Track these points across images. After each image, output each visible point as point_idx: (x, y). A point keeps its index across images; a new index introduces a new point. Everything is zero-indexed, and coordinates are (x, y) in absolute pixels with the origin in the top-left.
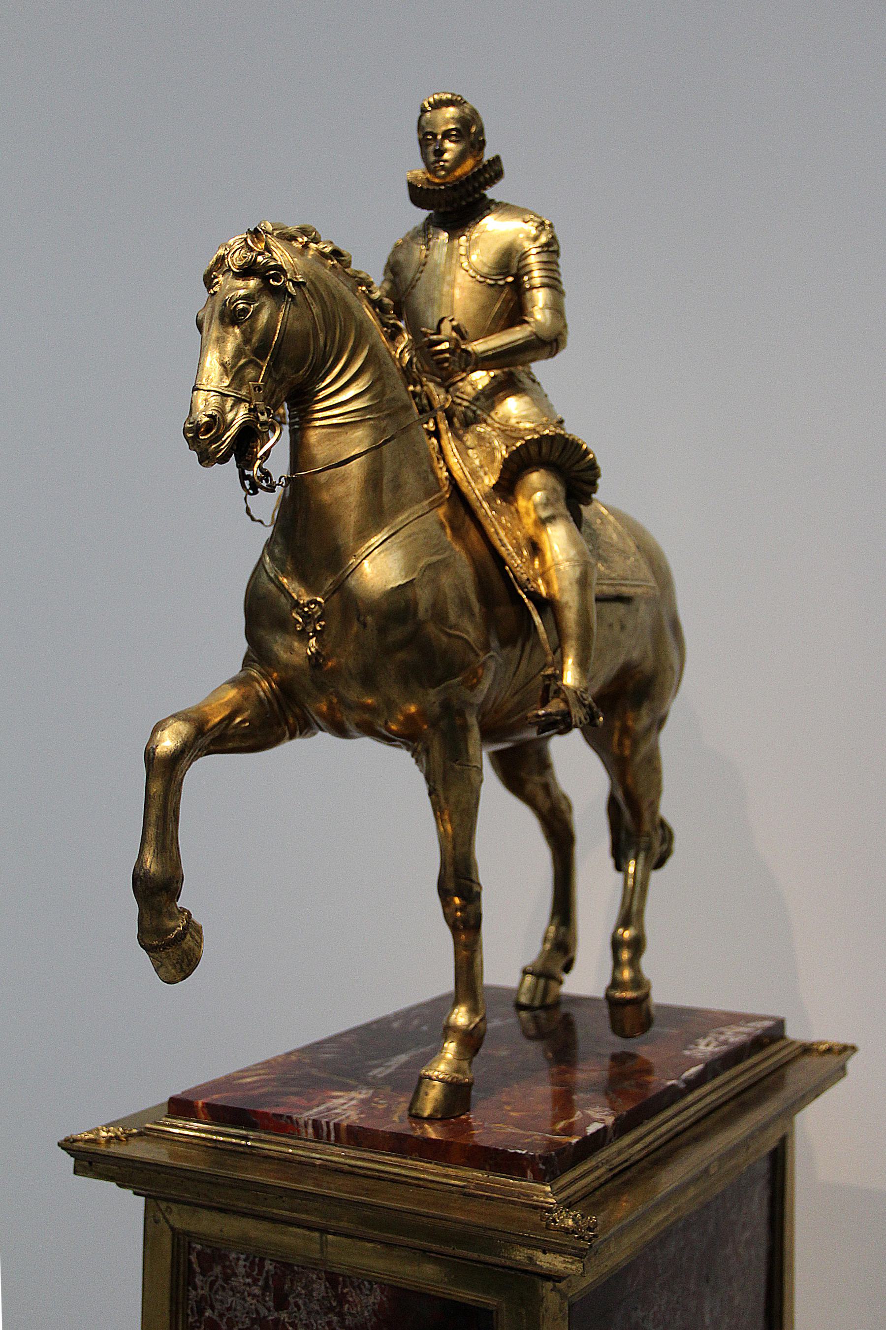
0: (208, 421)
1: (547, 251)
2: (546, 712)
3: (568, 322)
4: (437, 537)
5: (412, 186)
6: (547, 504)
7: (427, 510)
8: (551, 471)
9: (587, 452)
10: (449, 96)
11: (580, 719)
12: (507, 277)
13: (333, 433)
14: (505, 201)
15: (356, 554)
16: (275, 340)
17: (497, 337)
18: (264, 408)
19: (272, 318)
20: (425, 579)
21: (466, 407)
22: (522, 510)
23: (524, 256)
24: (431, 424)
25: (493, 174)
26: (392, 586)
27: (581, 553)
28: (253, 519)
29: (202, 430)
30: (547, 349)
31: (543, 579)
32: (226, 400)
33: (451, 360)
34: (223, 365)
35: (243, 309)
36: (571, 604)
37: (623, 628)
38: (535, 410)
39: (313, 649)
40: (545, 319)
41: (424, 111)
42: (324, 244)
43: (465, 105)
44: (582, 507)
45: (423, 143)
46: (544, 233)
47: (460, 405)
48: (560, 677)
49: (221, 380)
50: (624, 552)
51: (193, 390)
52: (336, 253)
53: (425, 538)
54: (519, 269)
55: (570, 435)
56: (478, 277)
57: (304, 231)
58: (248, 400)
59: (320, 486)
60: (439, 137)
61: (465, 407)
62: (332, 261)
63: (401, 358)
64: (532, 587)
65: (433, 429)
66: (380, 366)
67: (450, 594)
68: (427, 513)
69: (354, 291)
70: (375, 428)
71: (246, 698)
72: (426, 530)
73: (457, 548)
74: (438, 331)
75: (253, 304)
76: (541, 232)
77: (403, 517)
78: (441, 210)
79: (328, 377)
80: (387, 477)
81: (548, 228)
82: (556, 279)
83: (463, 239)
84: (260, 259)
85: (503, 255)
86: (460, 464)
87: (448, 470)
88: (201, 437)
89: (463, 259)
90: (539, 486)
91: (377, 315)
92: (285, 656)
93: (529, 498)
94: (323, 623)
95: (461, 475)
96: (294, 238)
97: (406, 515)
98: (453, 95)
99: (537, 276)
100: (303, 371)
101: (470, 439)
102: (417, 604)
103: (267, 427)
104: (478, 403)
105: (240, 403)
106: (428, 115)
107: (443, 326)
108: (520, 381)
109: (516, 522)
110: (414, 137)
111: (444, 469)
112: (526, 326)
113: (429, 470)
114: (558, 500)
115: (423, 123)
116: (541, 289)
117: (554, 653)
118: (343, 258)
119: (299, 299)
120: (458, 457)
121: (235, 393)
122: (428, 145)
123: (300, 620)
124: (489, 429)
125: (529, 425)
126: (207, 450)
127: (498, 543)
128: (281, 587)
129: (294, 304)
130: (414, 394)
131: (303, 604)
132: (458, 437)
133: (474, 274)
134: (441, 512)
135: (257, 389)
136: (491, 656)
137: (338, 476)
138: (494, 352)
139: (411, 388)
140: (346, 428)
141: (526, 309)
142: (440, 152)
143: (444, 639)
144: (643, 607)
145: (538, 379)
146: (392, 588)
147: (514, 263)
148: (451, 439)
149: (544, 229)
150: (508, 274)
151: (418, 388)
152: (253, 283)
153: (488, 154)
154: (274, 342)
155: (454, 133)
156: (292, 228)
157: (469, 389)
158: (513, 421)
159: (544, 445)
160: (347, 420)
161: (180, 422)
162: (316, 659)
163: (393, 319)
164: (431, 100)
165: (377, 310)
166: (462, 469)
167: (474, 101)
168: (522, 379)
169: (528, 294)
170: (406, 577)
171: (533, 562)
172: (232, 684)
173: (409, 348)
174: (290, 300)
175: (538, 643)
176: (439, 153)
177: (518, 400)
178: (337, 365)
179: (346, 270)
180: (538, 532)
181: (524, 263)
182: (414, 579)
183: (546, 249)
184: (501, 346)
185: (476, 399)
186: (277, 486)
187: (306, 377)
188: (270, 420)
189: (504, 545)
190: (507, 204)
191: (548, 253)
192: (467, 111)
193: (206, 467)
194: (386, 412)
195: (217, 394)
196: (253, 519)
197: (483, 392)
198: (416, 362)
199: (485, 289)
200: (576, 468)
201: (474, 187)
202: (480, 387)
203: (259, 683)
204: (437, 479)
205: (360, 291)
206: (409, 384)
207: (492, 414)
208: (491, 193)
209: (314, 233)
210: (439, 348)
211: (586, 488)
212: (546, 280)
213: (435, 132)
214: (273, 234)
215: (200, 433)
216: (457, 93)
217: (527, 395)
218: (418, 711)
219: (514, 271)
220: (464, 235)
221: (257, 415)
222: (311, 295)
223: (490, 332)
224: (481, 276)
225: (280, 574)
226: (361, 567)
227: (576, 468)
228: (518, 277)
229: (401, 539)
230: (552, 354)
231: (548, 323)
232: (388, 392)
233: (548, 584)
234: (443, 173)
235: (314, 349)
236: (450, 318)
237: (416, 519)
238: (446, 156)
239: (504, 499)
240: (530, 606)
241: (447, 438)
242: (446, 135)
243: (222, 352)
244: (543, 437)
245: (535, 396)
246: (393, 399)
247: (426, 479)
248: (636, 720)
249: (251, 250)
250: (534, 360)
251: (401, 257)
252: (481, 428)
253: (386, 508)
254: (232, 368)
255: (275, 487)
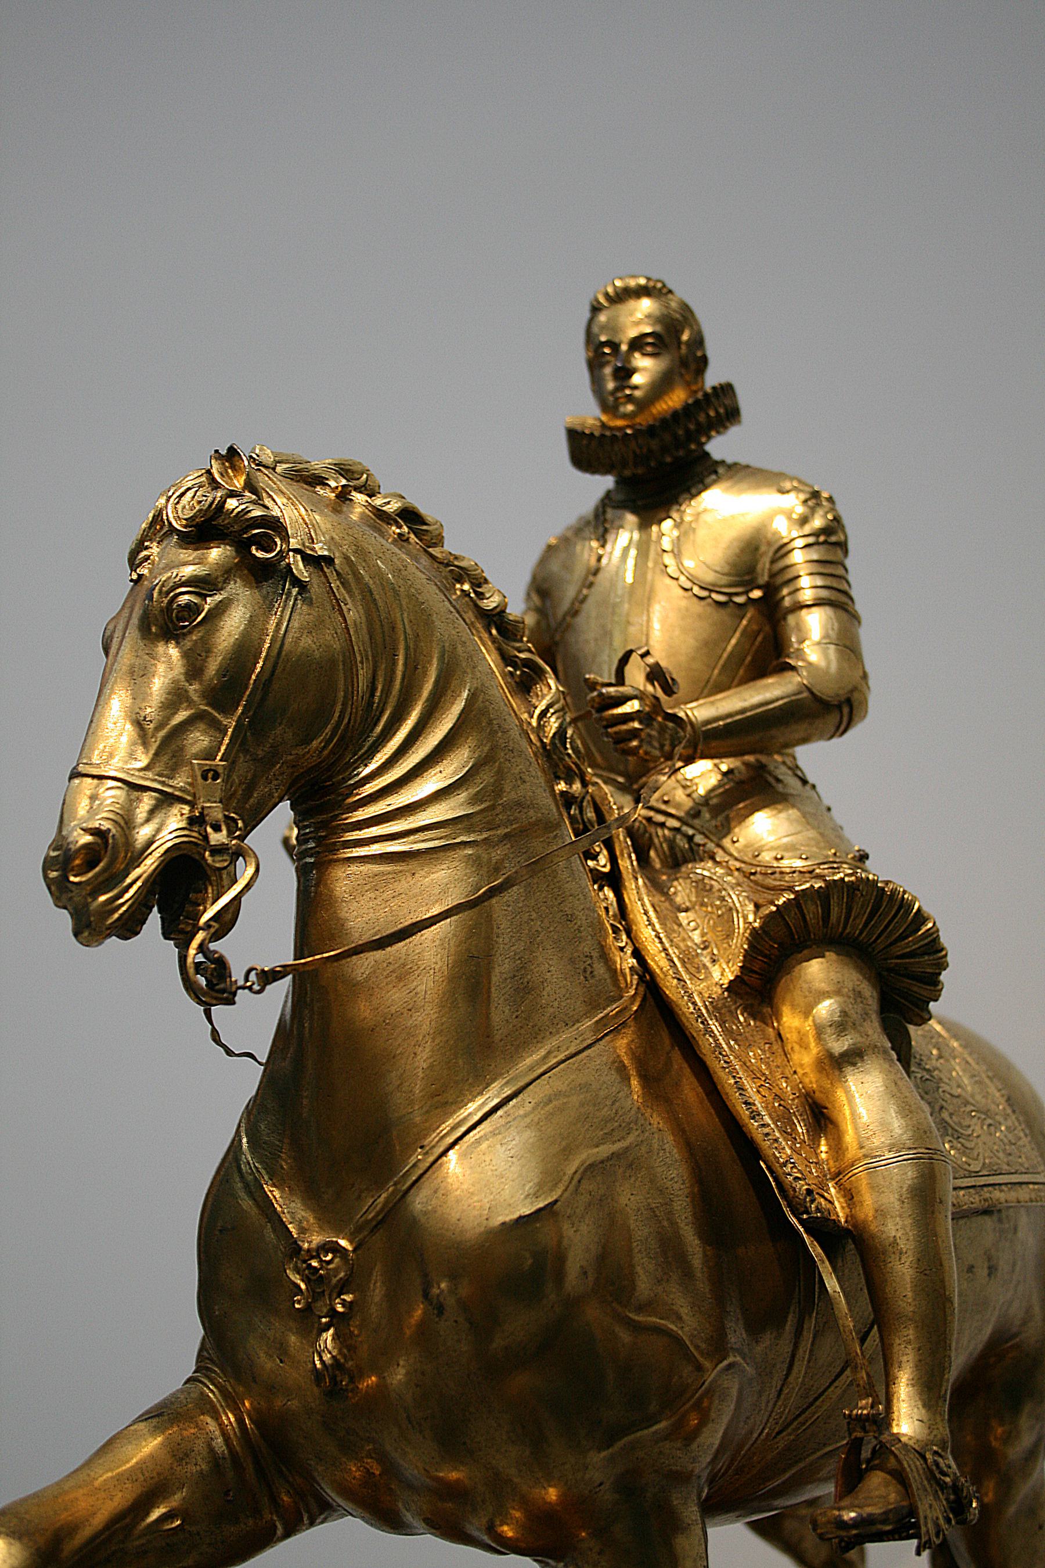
0: (89, 844)
1: (825, 542)
2: (860, 1515)
3: (868, 669)
4: (608, 1103)
5: (574, 436)
6: (841, 1026)
7: (589, 1042)
8: (848, 955)
9: (921, 918)
10: (642, 281)
11: (937, 1525)
12: (751, 590)
13: (383, 874)
14: (743, 461)
15: (426, 1143)
16: (258, 670)
17: (736, 693)
18: (220, 816)
19: (254, 625)
20: (583, 1199)
21: (677, 830)
22: (790, 1036)
23: (782, 550)
24: (603, 859)
25: (722, 411)
26: (501, 1219)
27: (920, 1133)
28: (229, 1052)
29: (77, 862)
30: (833, 719)
31: (839, 1185)
32: (139, 800)
33: (643, 735)
34: (139, 724)
35: (188, 606)
36: (902, 1245)
37: (992, 1270)
38: (812, 834)
39: (327, 1357)
40: (829, 663)
41: (596, 309)
42: (385, 498)
43: (670, 296)
44: (911, 1028)
45: (595, 364)
46: (820, 512)
47: (662, 825)
48: (883, 1421)
49: (131, 756)
50: (987, 1113)
51: (71, 778)
52: (410, 516)
53: (582, 1105)
54: (773, 575)
55: (887, 883)
56: (696, 590)
57: (344, 470)
58: (189, 798)
59: (354, 988)
60: (624, 347)
61: (670, 829)
62: (400, 527)
63: (540, 727)
64: (818, 1210)
65: (607, 870)
66: (493, 733)
67: (641, 1231)
68: (589, 1047)
69: (446, 590)
70: (476, 862)
71: (179, 1453)
72: (585, 1087)
73: (656, 1120)
74: (620, 680)
75: (210, 596)
76: (813, 510)
77: (535, 1057)
78: (627, 473)
79: (379, 755)
80: (502, 968)
81: (825, 503)
82: (845, 593)
83: (667, 525)
84: (231, 503)
85: (743, 550)
86: (661, 942)
87: (637, 954)
88: (72, 879)
89: (668, 559)
90: (824, 986)
91: (494, 640)
92: (269, 1365)
93: (807, 1013)
94: (348, 1298)
95: (664, 963)
96: (321, 481)
97: (542, 1052)
98: (648, 279)
99: (808, 587)
100: (319, 740)
101: (681, 891)
102: (561, 1259)
103: (225, 857)
104: (696, 822)
105: (171, 805)
106: (602, 318)
107: (629, 669)
108: (778, 780)
109: (780, 1060)
110: (579, 355)
111: (629, 951)
112: (789, 675)
113: (595, 954)
114: (865, 1016)
115: (595, 329)
116: (814, 609)
117: (863, 1340)
118: (425, 527)
119: (316, 589)
120: (658, 927)
121: (160, 782)
122: (602, 365)
123: (303, 1286)
124: (720, 871)
125: (798, 864)
126: (87, 905)
127: (743, 1112)
128: (266, 1206)
129: (304, 600)
130: (568, 800)
131: (309, 1250)
132: (658, 887)
133: (688, 585)
134: (622, 1044)
135: (210, 775)
136: (730, 1366)
137: (391, 968)
138: (729, 720)
139: (562, 786)
140: (413, 865)
141: (790, 644)
142: (625, 373)
143: (625, 1336)
144: (1023, 1220)
145: (811, 779)
146: (504, 1224)
147: (764, 565)
148: (643, 890)
149: (819, 505)
150: (752, 585)
151: (577, 787)
152: (216, 554)
153: (712, 379)
154: (254, 677)
155: (650, 340)
156: (318, 464)
157: (680, 795)
158: (767, 857)
159: (834, 902)
160: (416, 847)
161: (41, 848)
162: (333, 1378)
163: (529, 650)
164: (610, 290)
165: (494, 632)
166: (665, 949)
167: (683, 292)
168: (781, 777)
169: (791, 619)
170: (536, 1196)
171: (815, 1145)
172: (155, 1421)
173: (556, 707)
174: (295, 591)
175: (829, 1321)
176: (622, 374)
177: (774, 816)
178: (398, 730)
179: (430, 550)
180: (827, 1084)
181: (781, 564)
182: (556, 1201)
183: (822, 539)
184: (743, 711)
185: (695, 813)
186: (240, 991)
187: (326, 752)
188: (234, 842)
189: (755, 1115)
190: (748, 467)
191: (825, 546)
192: (673, 304)
193: (87, 946)
194: (501, 831)
195: (119, 784)
196: (229, 1052)
197: (706, 800)
198: (572, 737)
199: (709, 609)
200: (897, 950)
201: (687, 431)
202: (702, 791)
203: (217, 1418)
204: (614, 972)
205: (458, 593)
206: (558, 778)
207: (726, 842)
208: (718, 447)
209: (365, 476)
210: (620, 710)
211: (918, 988)
212: (824, 593)
213: (617, 340)
214: (274, 469)
215: (72, 870)
216: (654, 276)
217: (793, 806)
218: (563, 1497)
219: (764, 579)
220: (670, 517)
221: (206, 831)
222: (344, 584)
223: (720, 688)
224: (702, 588)
225: (266, 1178)
226: (441, 1165)
227: (897, 950)
228: (771, 590)
229: (528, 1107)
230: (841, 729)
231: (834, 667)
232: (507, 788)
233: (850, 1196)
234: (630, 408)
235: (345, 697)
236: (643, 650)
237: (563, 1061)
238: (637, 379)
239: (753, 1013)
240: (815, 1250)
241: (636, 889)
242: (637, 344)
243: (139, 695)
244: (831, 885)
245: (810, 809)
246: (519, 804)
247: (588, 973)
248: (1009, 1438)
249: (215, 485)
250: (805, 740)
251: (555, 566)
252: (704, 869)
253: (497, 1037)
254: (158, 729)
255: (235, 994)
